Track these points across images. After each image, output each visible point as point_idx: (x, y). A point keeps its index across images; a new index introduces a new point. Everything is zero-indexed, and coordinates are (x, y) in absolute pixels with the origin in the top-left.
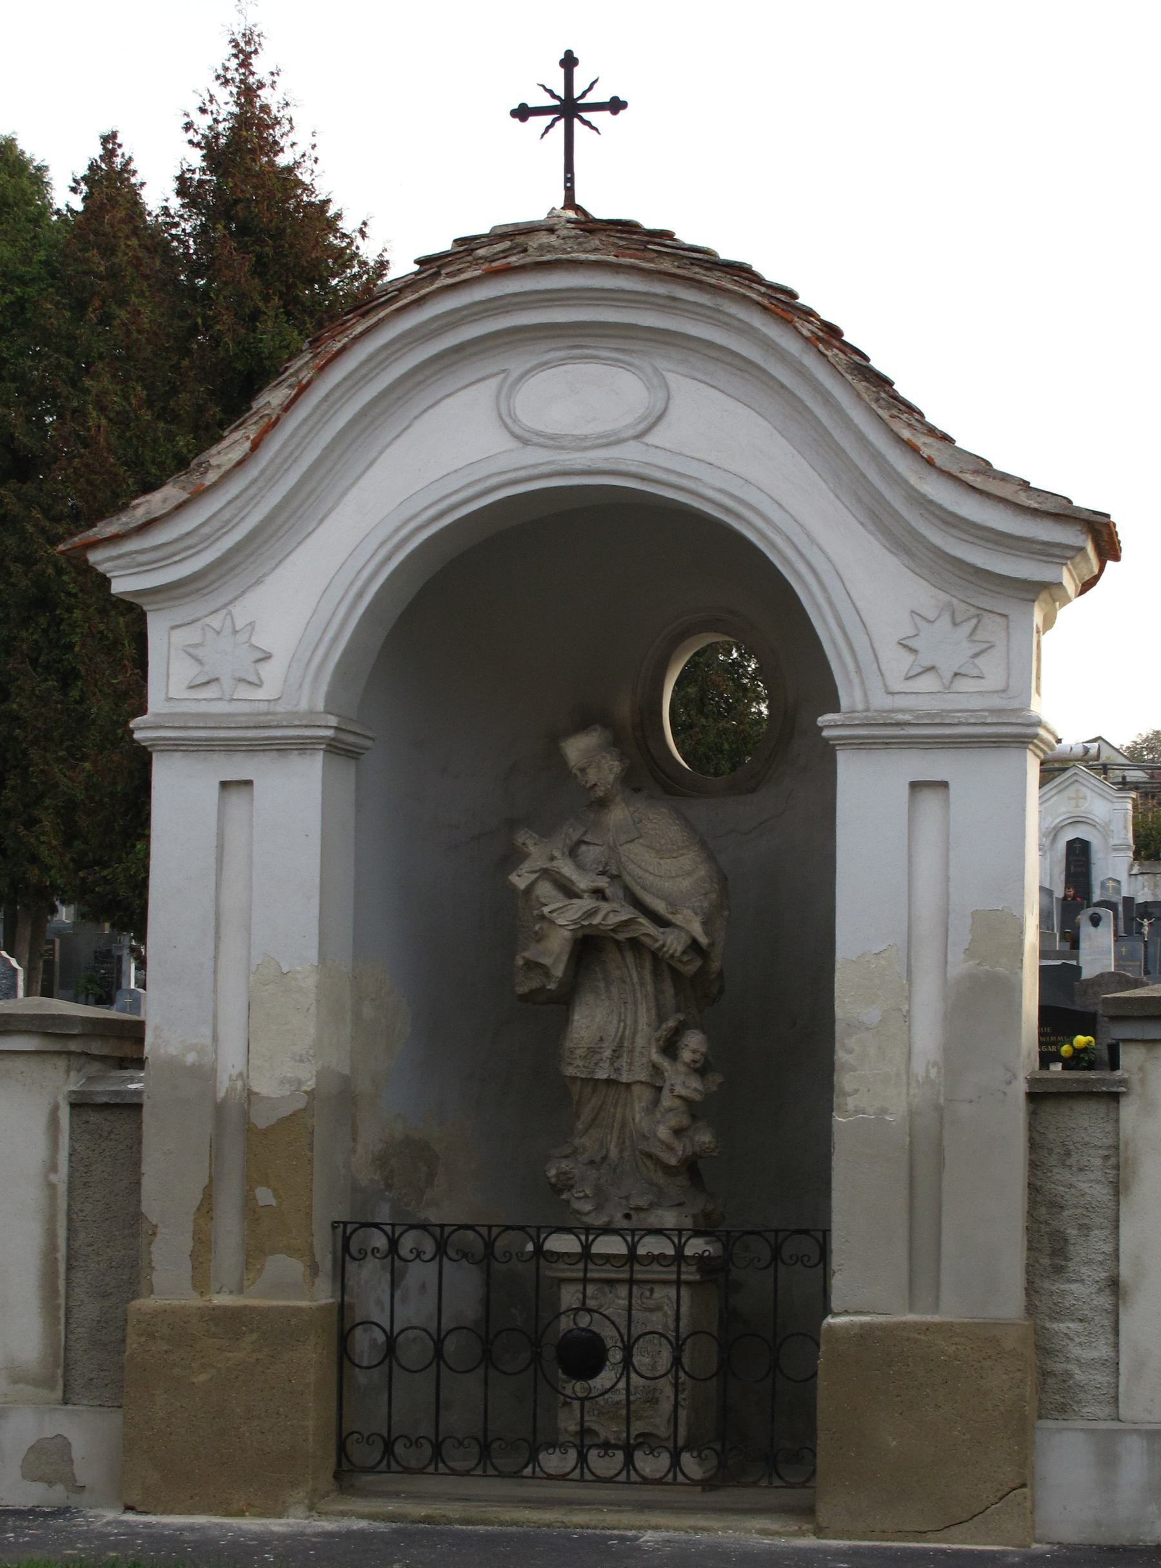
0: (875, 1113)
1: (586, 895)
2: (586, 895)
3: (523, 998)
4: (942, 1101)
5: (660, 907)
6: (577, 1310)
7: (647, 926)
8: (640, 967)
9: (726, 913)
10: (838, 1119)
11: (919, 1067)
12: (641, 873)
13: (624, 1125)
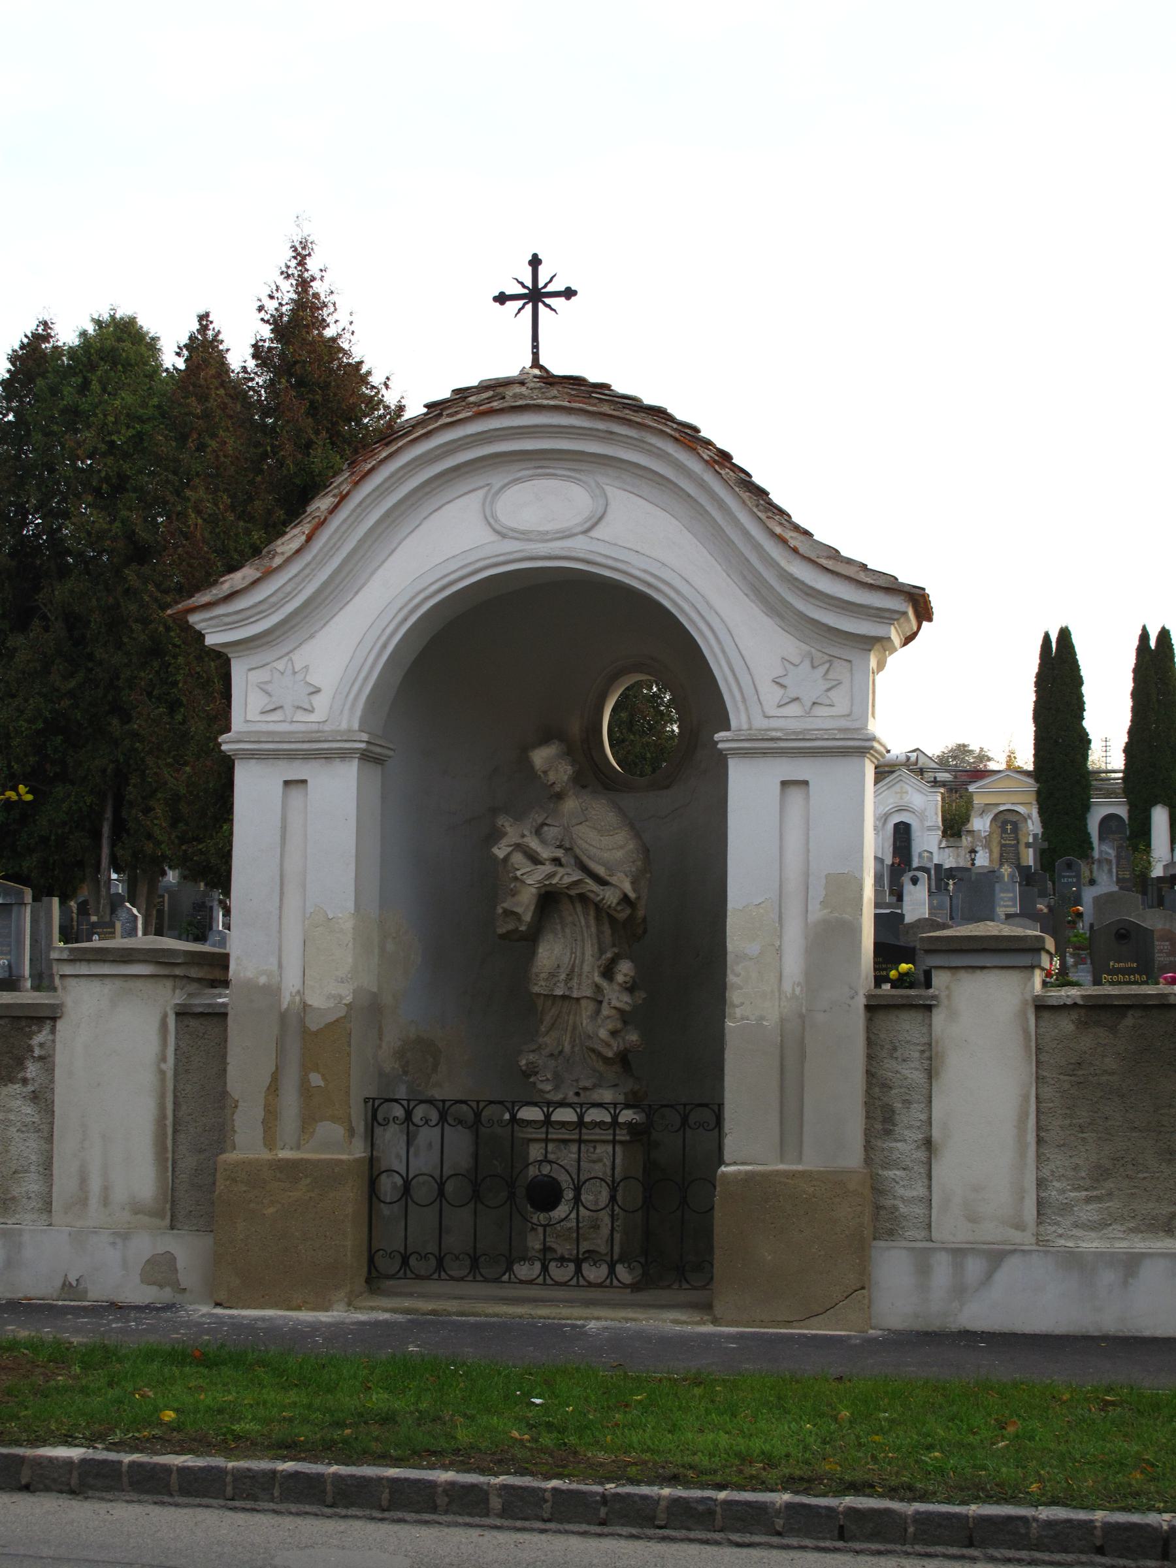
3: (503, 937)
4: (804, 1011)
5: (601, 871)
7: (591, 885)
8: (586, 914)
10: (729, 1024)
11: (787, 987)
13: (574, 1028)
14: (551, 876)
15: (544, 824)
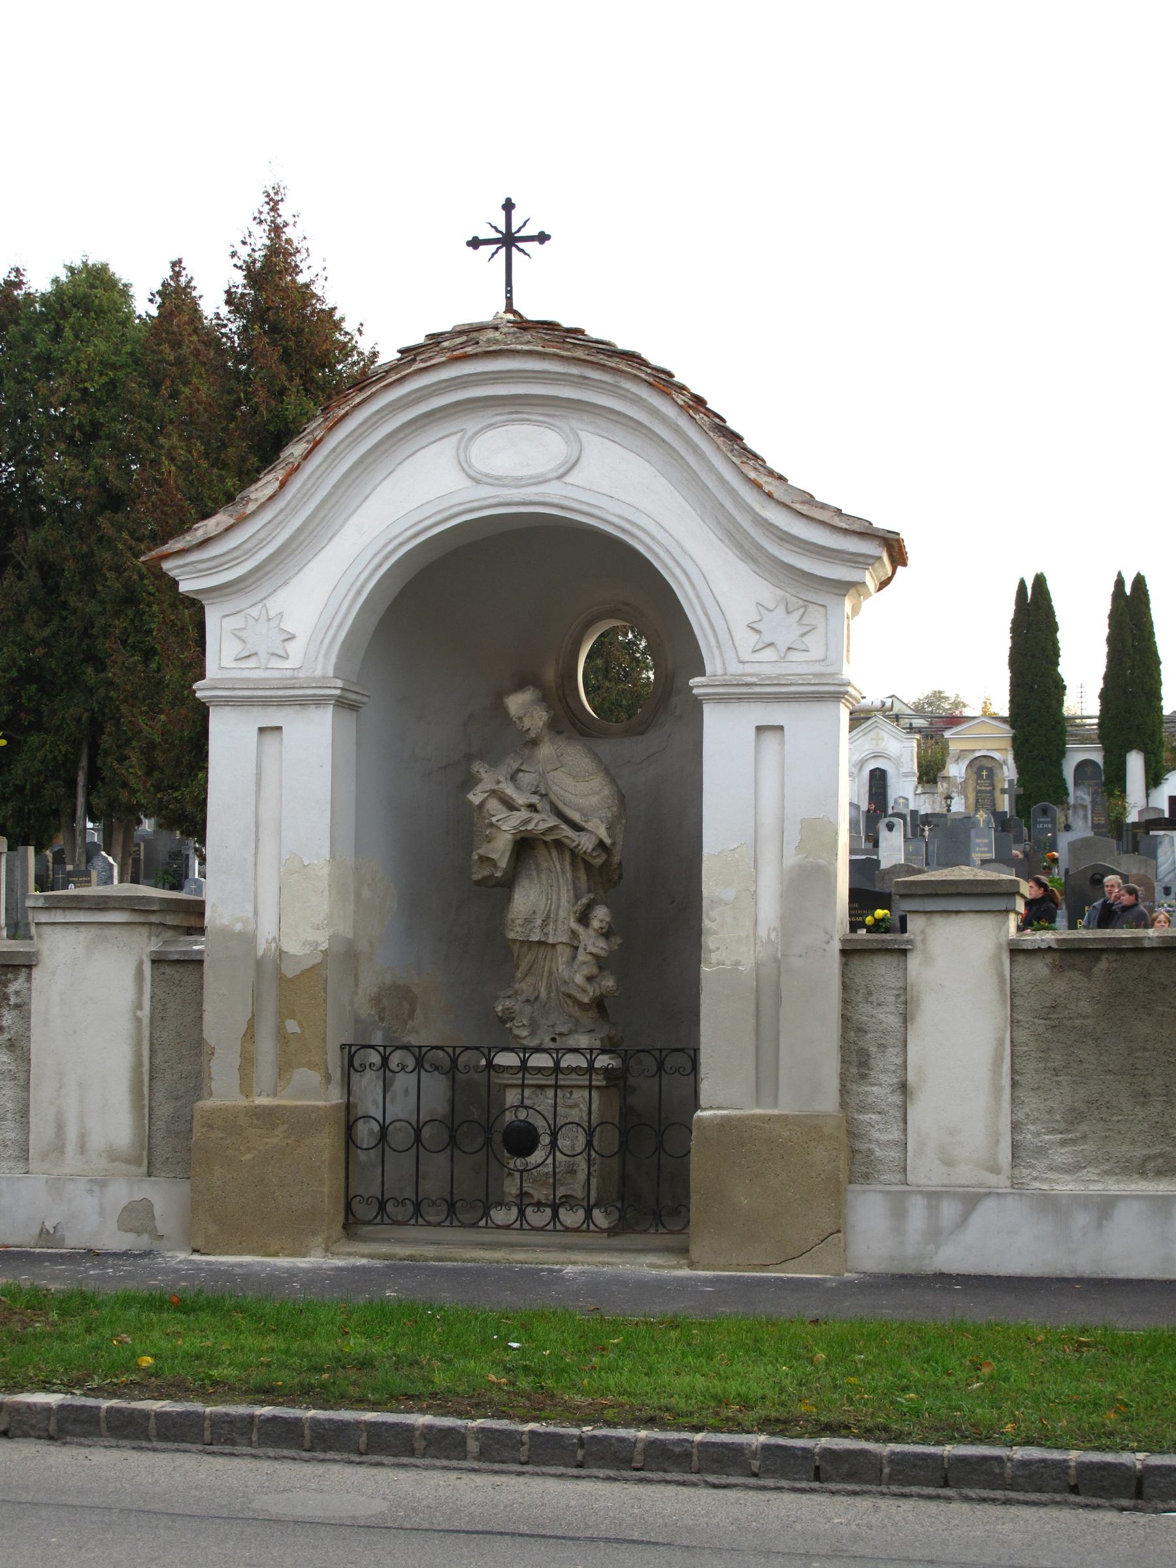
3: (478, 883)
4: (779, 955)
5: (576, 817)
6: (518, 1107)
7: (567, 831)
9: (624, 821)
10: (705, 969)
11: (763, 932)
13: (551, 973)
14: (526, 822)
15: (519, 770)
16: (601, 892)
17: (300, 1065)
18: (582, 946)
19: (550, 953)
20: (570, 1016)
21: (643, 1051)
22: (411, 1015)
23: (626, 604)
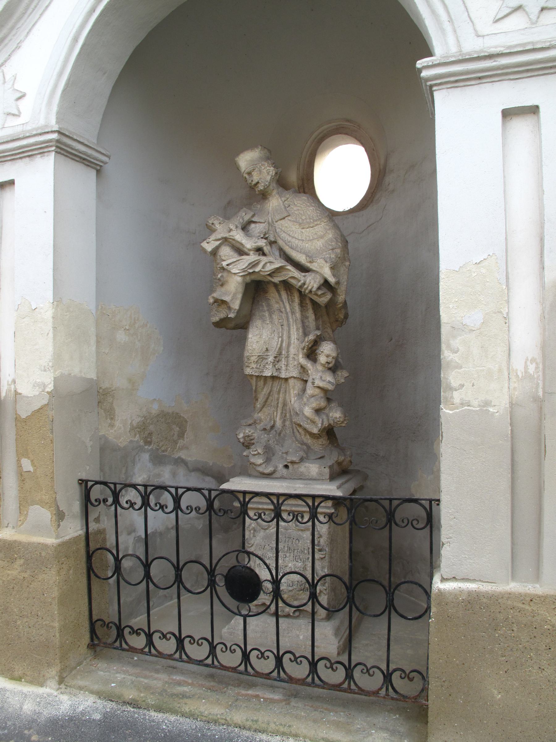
0: (479, 406)
1: (251, 253)
2: (251, 253)
4: (541, 393)
5: (302, 259)
6: (239, 551)
7: (293, 272)
8: (291, 301)
9: (347, 263)
10: (445, 411)
11: (518, 365)
12: (290, 239)
13: (285, 404)
14: (254, 264)
15: (250, 222)
16: (329, 331)
17: (34, 503)
18: (310, 380)
19: (283, 387)
20: (303, 443)
21: (371, 500)
22: (181, 435)
23: (348, 121)
